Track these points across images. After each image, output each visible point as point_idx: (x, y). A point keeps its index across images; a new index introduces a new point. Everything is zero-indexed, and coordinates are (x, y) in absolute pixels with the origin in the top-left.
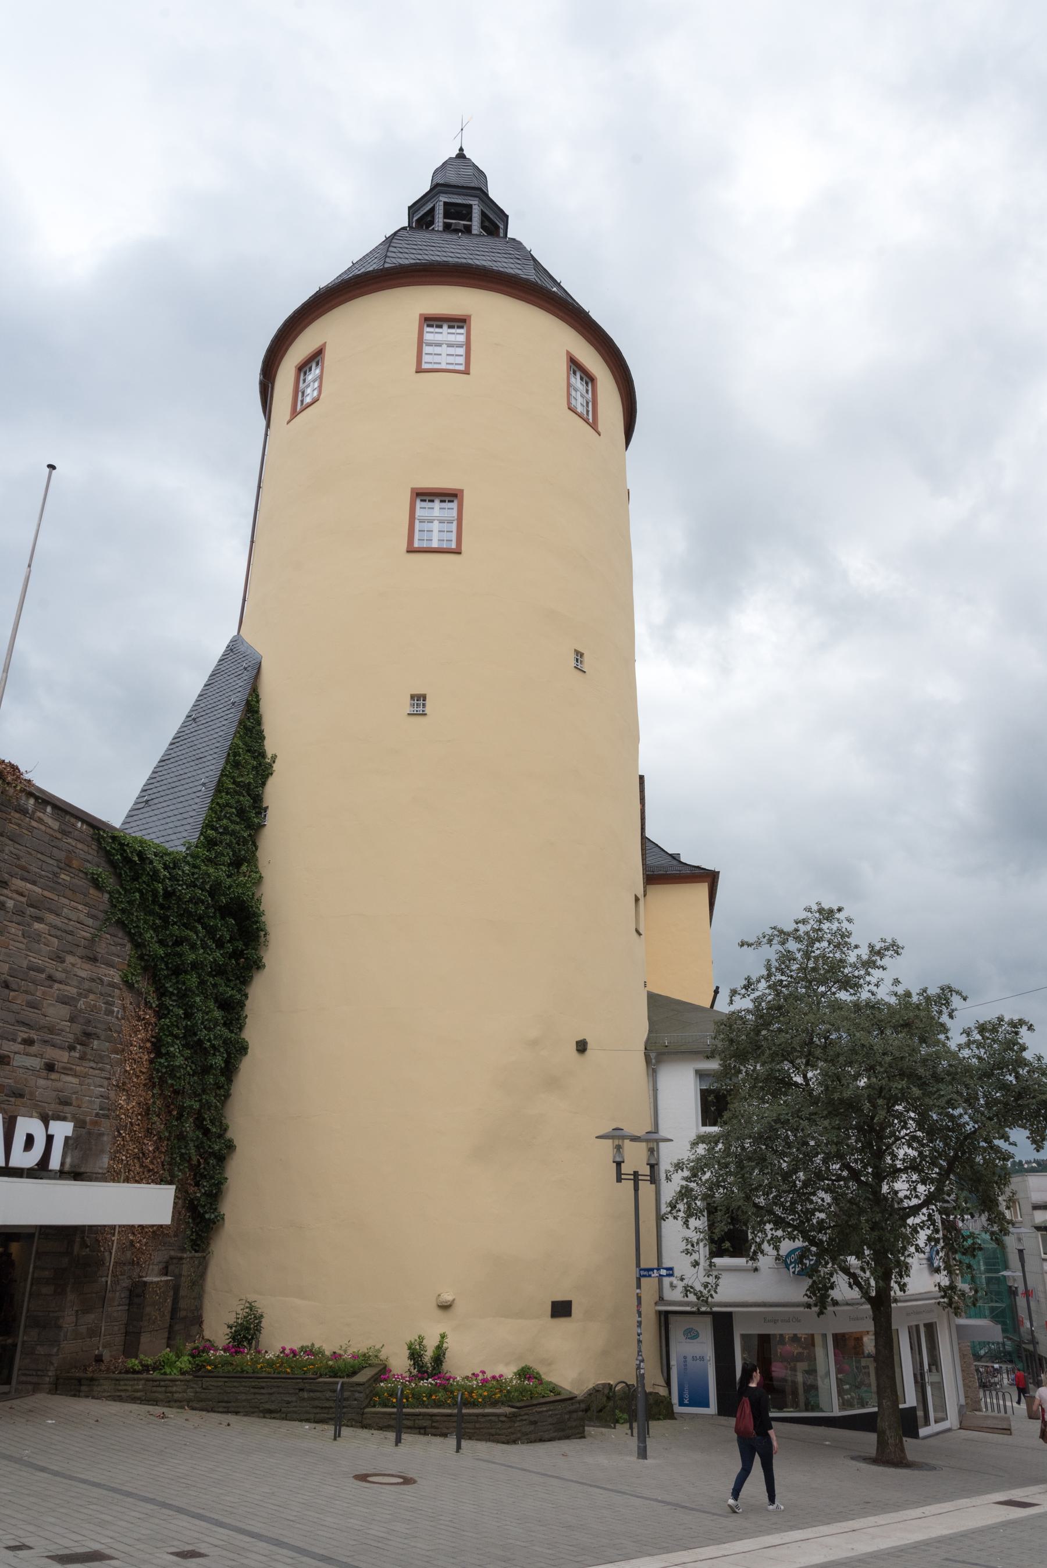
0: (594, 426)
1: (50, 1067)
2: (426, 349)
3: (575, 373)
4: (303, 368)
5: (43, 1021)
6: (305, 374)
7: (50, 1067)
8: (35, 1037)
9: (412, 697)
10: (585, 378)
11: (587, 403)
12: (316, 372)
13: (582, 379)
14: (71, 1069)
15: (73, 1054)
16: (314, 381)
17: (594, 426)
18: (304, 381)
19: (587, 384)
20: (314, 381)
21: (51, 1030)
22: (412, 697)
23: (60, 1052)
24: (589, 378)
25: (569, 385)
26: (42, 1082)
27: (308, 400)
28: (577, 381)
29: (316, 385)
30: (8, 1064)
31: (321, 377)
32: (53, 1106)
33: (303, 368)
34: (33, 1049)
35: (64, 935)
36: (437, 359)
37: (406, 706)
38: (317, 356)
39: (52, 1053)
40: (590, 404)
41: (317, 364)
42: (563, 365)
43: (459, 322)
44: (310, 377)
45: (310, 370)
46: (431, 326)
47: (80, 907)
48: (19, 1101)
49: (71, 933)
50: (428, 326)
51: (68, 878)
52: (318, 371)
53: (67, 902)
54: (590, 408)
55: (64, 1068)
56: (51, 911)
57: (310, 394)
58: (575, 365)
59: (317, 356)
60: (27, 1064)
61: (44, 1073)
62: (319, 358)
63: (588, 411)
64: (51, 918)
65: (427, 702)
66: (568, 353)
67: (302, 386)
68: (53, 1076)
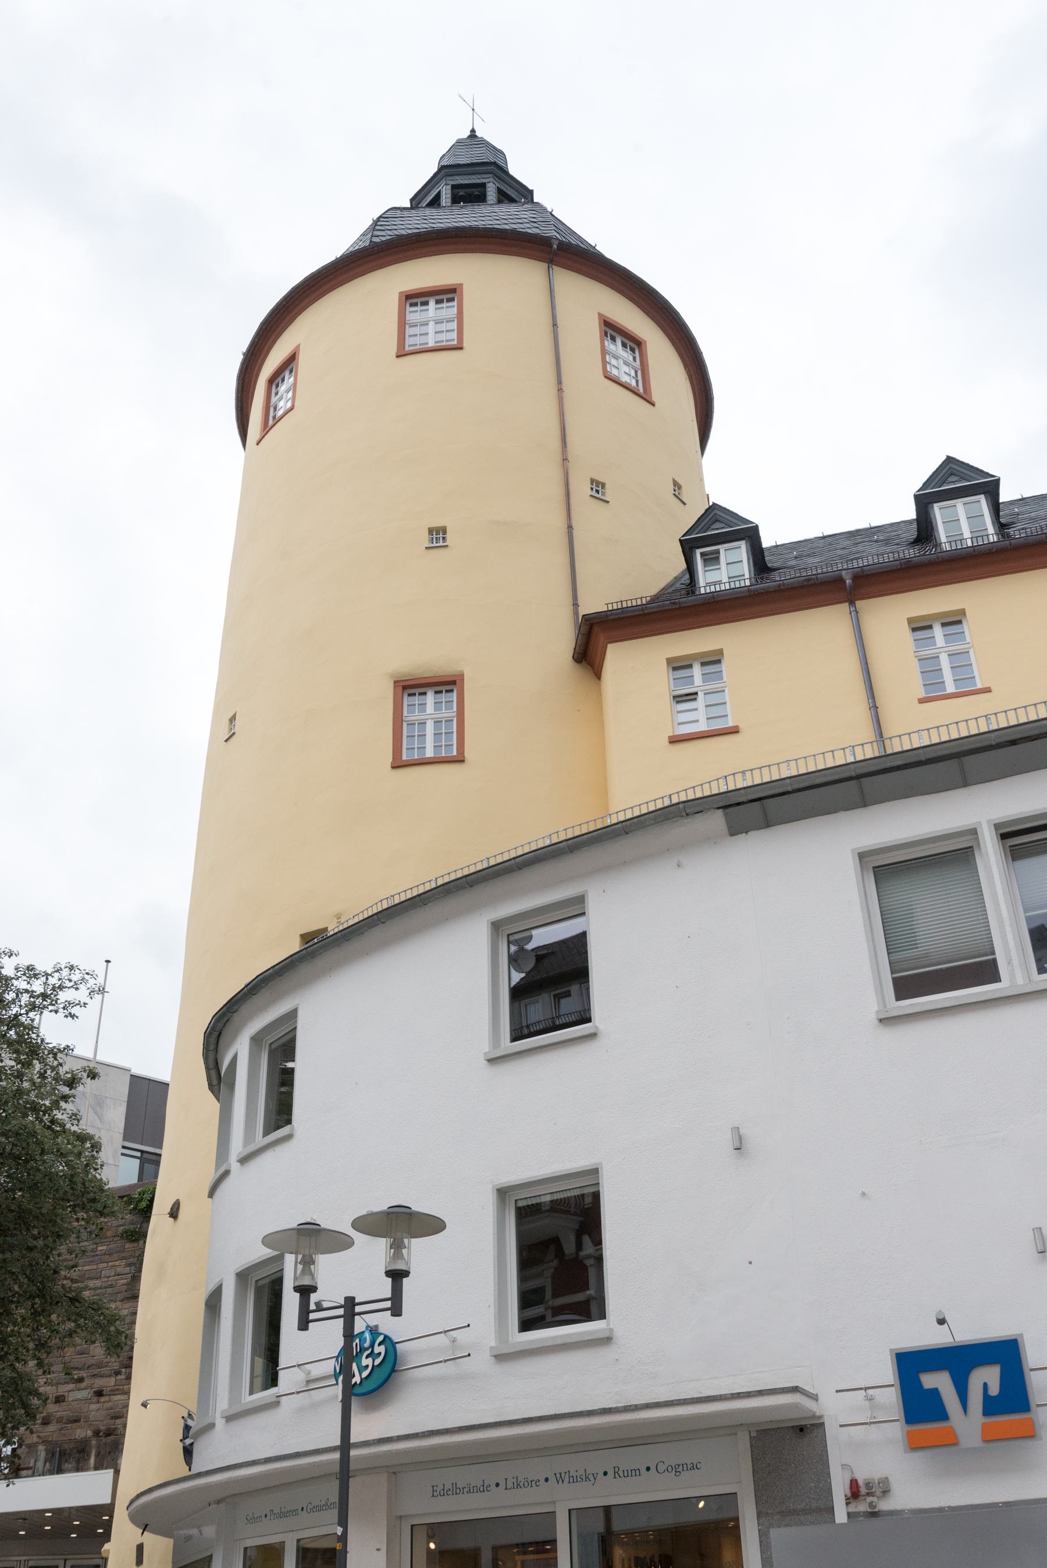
0: (646, 397)
1: (99, 1394)
2: (409, 331)
3: (613, 339)
4: (275, 379)
5: (92, 1361)
6: (277, 386)
7: (99, 1394)
8: (85, 1375)
9: (431, 531)
10: (629, 343)
11: (636, 372)
12: (289, 381)
13: (624, 345)
14: (118, 1390)
15: (119, 1377)
16: (288, 391)
17: (646, 397)
18: (277, 394)
19: (633, 350)
20: (288, 391)
21: (99, 1365)
22: (431, 531)
23: (107, 1379)
24: (634, 343)
25: (604, 352)
26: (94, 1407)
27: (280, 413)
28: (616, 348)
29: (290, 395)
30: (64, 1401)
31: (295, 384)
32: (105, 1422)
33: (275, 379)
34: (83, 1385)
35: (103, 1291)
36: (423, 339)
37: (424, 539)
38: (290, 363)
39: (99, 1383)
40: (639, 373)
41: (291, 372)
42: (595, 328)
43: (448, 294)
44: (283, 388)
45: (283, 380)
46: (415, 305)
47: (117, 1263)
48: (75, 1425)
49: (111, 1286)
50: (412, 305)
51: (104, 1248)
52: (292, 379)
53: (105, 1265)
54: (640, 378)
55: (113, 1391)
56: (91, 1279)
57: (283, 405)
58: (611, 329)
59: (290, 363)
60: (79, 1397)
61: (95, 1399)
62: (293, 365)
63: (637, 381)
64: (91, 1284)
65: (448, 536)
66: (600, 315)
67: (274, 399)
68: (103, 1399)
